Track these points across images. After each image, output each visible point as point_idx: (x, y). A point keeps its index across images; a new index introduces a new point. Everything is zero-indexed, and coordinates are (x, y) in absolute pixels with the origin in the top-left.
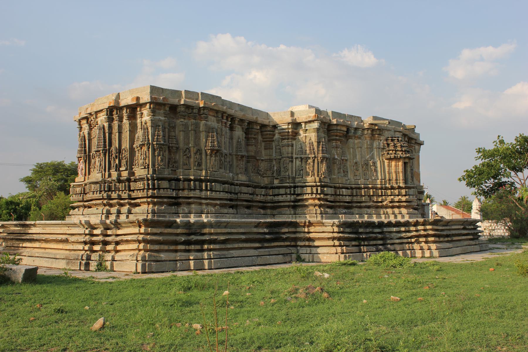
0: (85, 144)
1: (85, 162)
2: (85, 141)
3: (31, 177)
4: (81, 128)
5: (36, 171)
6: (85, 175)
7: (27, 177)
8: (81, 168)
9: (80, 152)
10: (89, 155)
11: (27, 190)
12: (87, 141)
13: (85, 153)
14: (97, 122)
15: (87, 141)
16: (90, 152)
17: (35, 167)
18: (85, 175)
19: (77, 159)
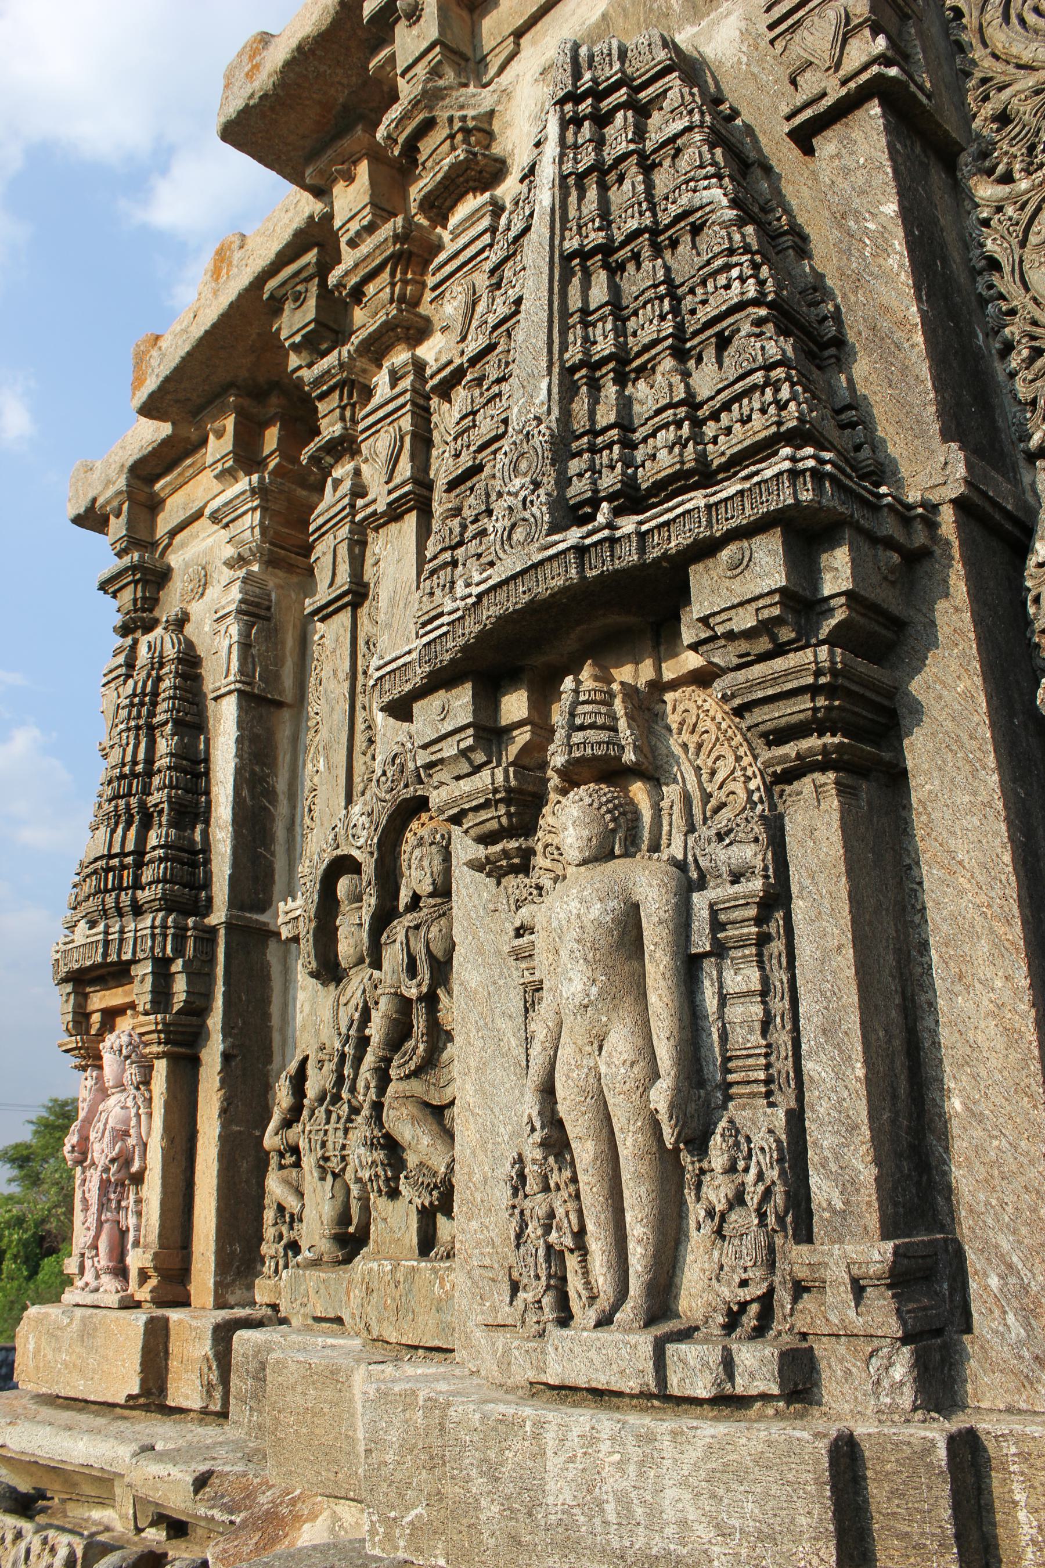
0: (193, 768)
1: (183, 1044)
2: (192, 723)
3: (28, 1147)
4: (153, 578)
5: (46, 1126)
6: (173, 1282)
7: (16, 1146)
8: (101, 1151)
9: (110, 881)
10: (252, 938)
11: (15, 1189)
12: (225, 723)
13: (187, 893)
14: (482, 130)
15: (225, 723)
16: (256, 882)
17: (46, 1115)
18: (173, 1282)
19: (56, 1004)
